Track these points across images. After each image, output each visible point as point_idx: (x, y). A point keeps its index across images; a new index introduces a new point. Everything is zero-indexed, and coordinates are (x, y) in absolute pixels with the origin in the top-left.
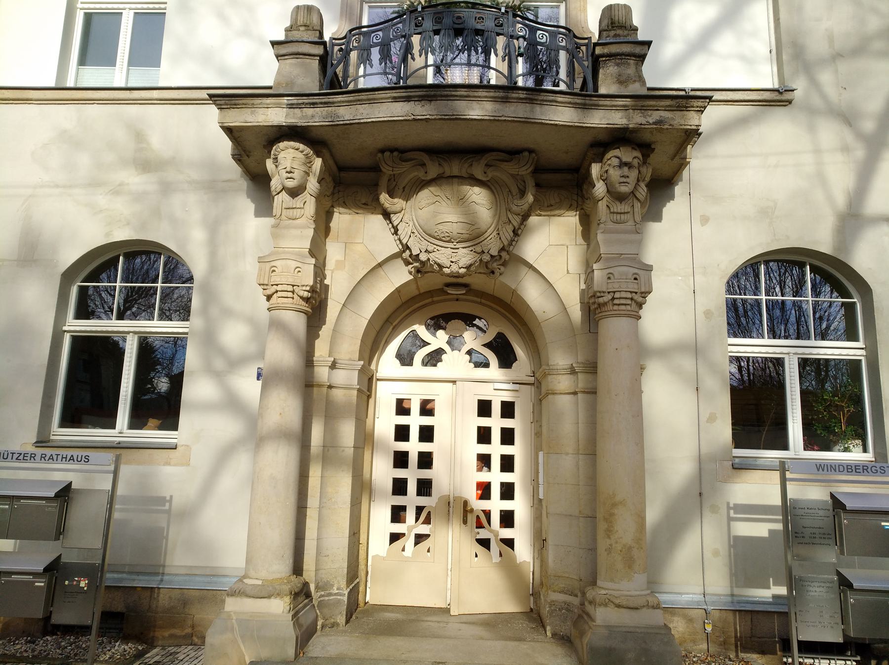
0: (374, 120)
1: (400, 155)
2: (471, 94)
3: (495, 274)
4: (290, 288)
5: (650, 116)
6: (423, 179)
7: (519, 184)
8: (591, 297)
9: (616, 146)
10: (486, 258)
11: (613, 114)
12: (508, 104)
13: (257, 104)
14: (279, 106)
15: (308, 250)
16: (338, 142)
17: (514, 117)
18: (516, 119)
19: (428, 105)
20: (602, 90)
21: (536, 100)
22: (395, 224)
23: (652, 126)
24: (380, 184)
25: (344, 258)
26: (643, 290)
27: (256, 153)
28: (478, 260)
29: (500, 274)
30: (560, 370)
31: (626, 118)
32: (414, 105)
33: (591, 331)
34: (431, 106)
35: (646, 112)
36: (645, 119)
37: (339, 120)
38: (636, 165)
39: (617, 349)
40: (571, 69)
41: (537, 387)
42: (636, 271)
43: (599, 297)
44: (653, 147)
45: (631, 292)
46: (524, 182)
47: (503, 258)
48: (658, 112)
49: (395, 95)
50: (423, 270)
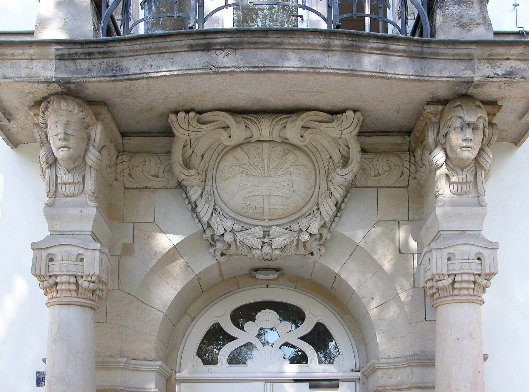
0: (166, 73)
1: (198, 116)
2: (286, 41)
3: (315, 255)
4: (73, 280)
5: (499, 67)
6: (227, 144)
7: (341, 150)
8: (429, 280)
9: (457, 104)
10: (305, 237)
11: (455, 65)
12: (330, 53)
13: (18, 55)
14: (46, 57)
15: (90, 233)
16: (121, 101)
17: (337, 69)
18: (340, 72)
19: (233, 54)
20: (440, 36)
21: (365, 48)
22: (193, 199)
23: (501, 79)
24: (173, 152)
25: (132, 241)
26: (487, 271)
27: (18, 116)
28: (295, 240)
29: (320, 255)
30: (392, 363)
31: (470, 69)
32: (215, 55)
33: (426, 320)
34: (237, 56)
35: (494, 63)
36: (493, 70)
37: (122, 74)
38: (481, 126)
39: (458, 339)
40: (403, 9)
41: (364, 383)
42: (479, 250)
43: (438, 281)
44: (499, 103)
45: (474, 275)
46: (348, 147)
47: (324, 236)
48: (508, 61)
49: (192, 42)
50: (227, 252)
